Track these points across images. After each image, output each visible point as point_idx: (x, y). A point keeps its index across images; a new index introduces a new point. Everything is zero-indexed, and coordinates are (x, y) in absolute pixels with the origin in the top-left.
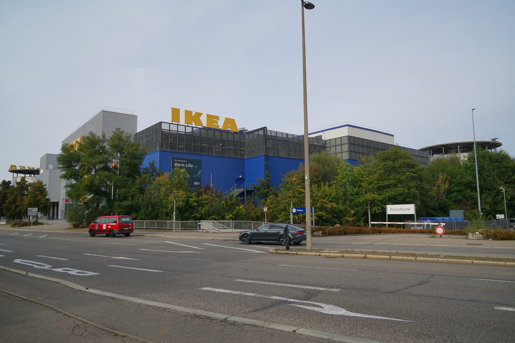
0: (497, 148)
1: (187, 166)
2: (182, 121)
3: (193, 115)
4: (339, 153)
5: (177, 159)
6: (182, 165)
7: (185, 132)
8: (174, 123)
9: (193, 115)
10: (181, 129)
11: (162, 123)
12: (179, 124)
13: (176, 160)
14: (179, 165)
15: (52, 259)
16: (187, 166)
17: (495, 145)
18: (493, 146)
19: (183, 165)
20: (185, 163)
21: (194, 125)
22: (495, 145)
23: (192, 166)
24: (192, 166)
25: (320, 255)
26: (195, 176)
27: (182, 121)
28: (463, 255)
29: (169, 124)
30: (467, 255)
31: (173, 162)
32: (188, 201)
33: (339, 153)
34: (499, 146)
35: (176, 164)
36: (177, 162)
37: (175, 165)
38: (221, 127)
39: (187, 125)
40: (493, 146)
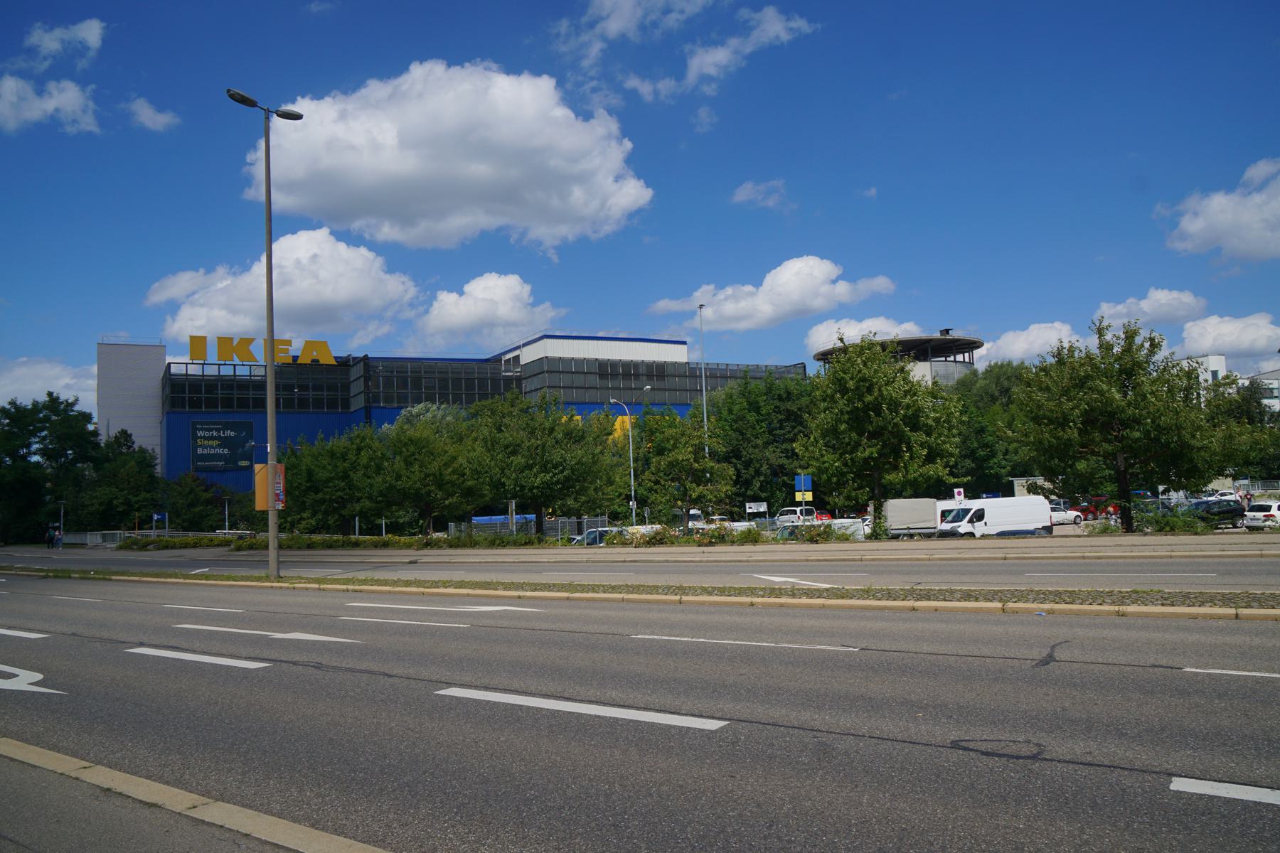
0: (974, 352)
1: (224, 433)
2: (212, 356)
3: (234, 345)
4: (955, 359)
5: (198, 423)
6: (213, 434)
7: (250, 376)
8: (194, 362)
9: (234, 345)
10: (211, 371)
11: (172, 365)
12: (206, 362)
13: (200, 427)
14: (207, 434)
15: (337, 637)
16: (224, 433)
17: (971, 346)
18: (967, 346)
19: (214, 434)
20: (218, 430)
21: (237, 361)
22: (971, 346)
23: (232, 434)
24: (232, 434)
25: (1237, 616)
26: (241, 449)
27: (212, 356)
28: (651, 580)
29: (185, 365)
30: (661, 581)
31: (195, 429)
32: (110, 502)
33: (955, 359)
34: (978, 347)
35: (200, 433)
36: (202, 429)
37: (199, 435)
38: (96, 382)
39: (223, 362)
40: (967, 346)
